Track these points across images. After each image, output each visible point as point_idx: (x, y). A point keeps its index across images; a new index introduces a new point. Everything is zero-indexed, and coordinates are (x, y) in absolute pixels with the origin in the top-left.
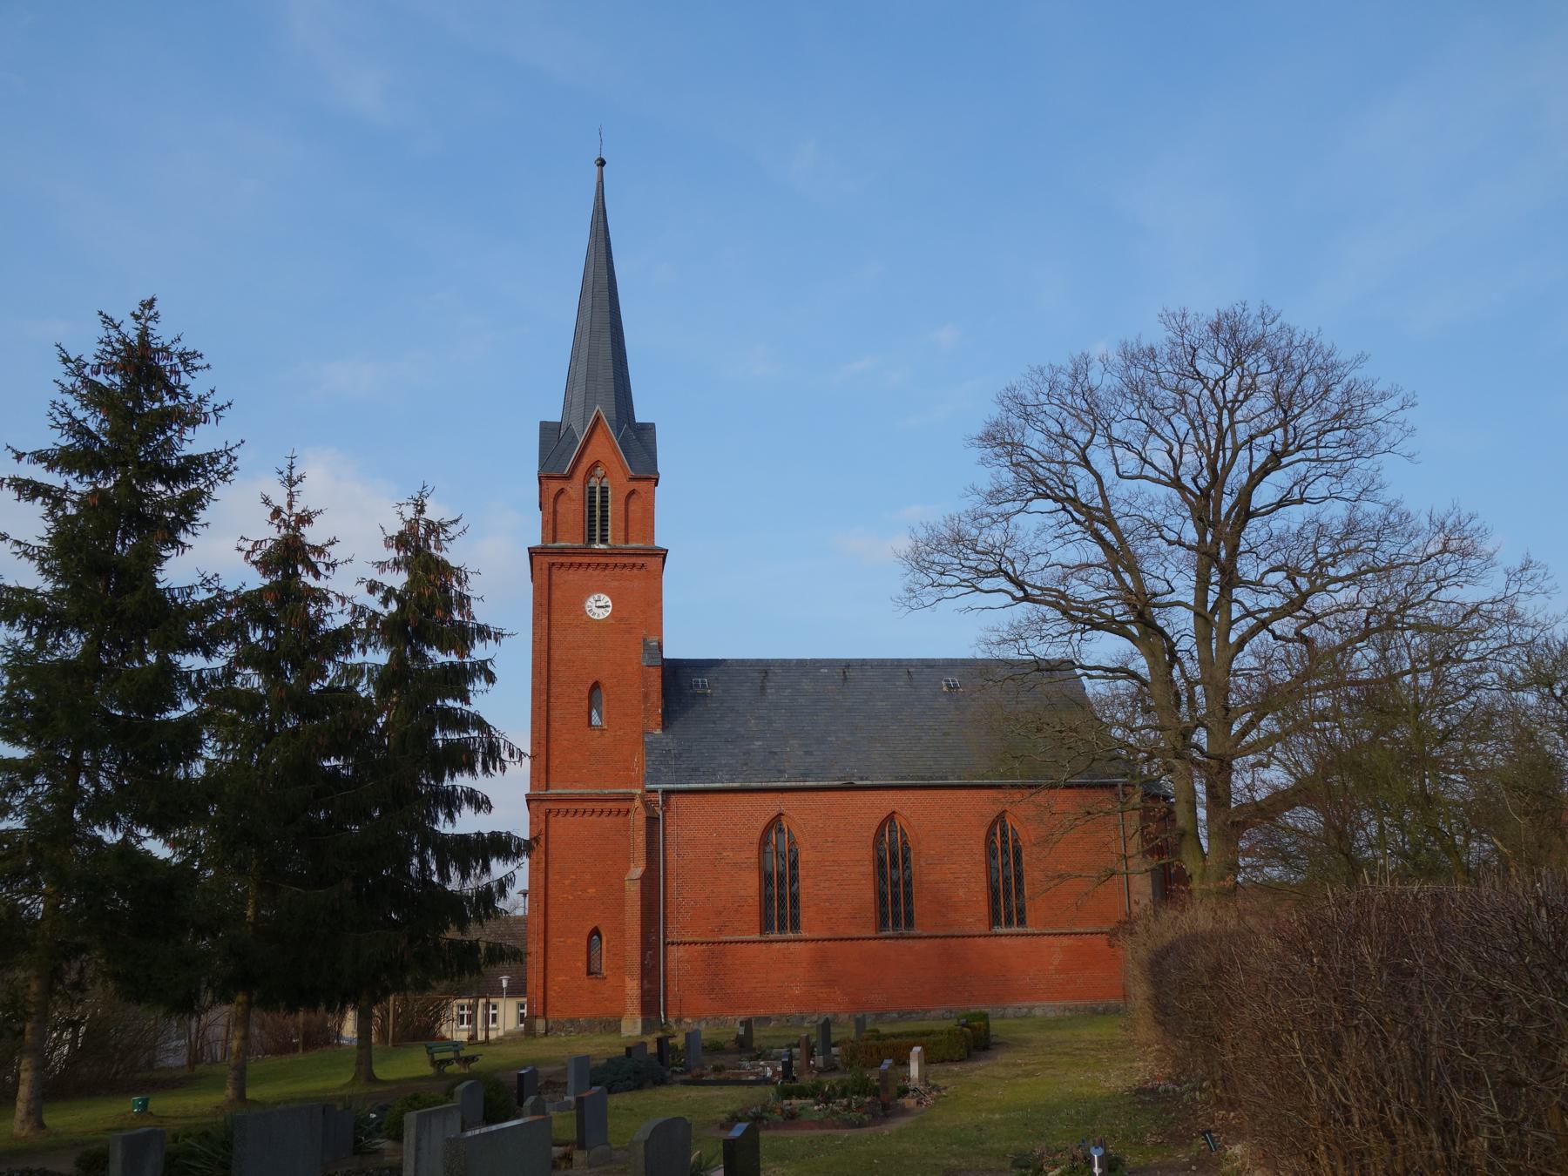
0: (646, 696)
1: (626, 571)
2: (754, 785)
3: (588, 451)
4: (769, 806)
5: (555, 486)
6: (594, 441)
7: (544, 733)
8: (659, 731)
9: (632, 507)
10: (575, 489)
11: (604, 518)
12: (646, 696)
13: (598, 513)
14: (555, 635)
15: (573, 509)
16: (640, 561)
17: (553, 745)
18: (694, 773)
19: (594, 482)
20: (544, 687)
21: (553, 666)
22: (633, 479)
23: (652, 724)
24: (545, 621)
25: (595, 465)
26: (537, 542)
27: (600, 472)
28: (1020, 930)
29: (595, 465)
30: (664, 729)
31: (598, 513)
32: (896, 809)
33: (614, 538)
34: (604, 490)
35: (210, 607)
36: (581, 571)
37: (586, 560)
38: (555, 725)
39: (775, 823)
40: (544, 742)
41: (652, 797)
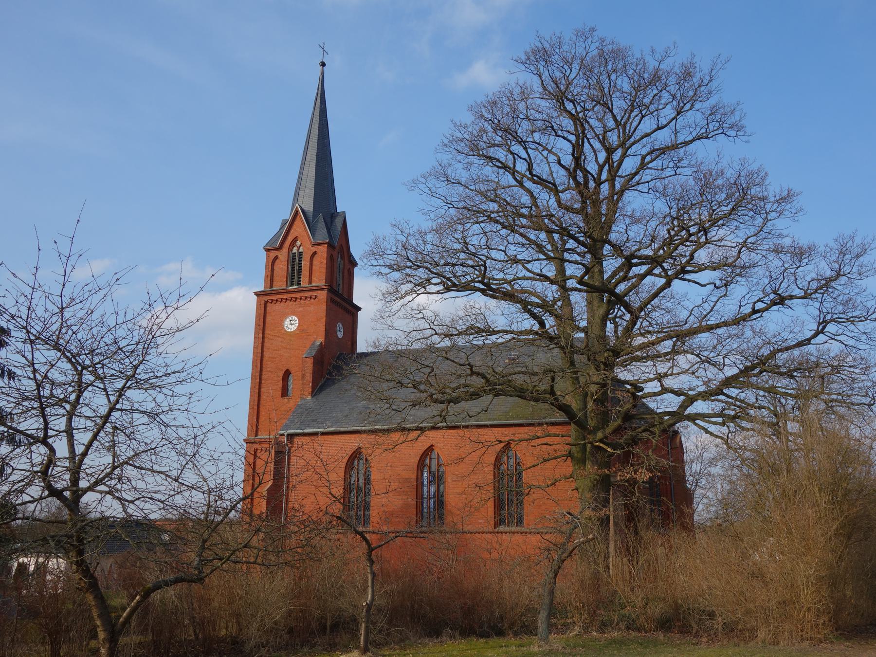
0: (303, 376)
1: (307, 301)
2: (306, 431)
3: (292, 231)
4: (352, 443)
5: (273, 254)
6: (295, 225)
7: (256, 402)
8: (309, 398)
9: (315, 262)
10: (283, 255)
11: (300, 271)
12: (303, 376)
13: (297, 268)
14: (266, 343)
15: (281, 268)
16: (314, 294)
17: (261, 409)
18: (315, 422)
19: (295, 250)
20: (258, 374)
21: (264, 361)
22: (315, 245)
23: (306, 394)
24: (261, 335)
25: (295, 240)
26: (261, 288)
27: (298, 243)
28: (518, 529)
29: (295, 240)
30: (312, 397)
31: (297, 268)
32: (434, 443)
33: (304, 283)
34: (300, 254)
35: (818, 365)
36: (283, 304)
37: (285, 296)
38: (263, 397)
39: (356, 454)
40: (256, 407)
41: (282, 438)
